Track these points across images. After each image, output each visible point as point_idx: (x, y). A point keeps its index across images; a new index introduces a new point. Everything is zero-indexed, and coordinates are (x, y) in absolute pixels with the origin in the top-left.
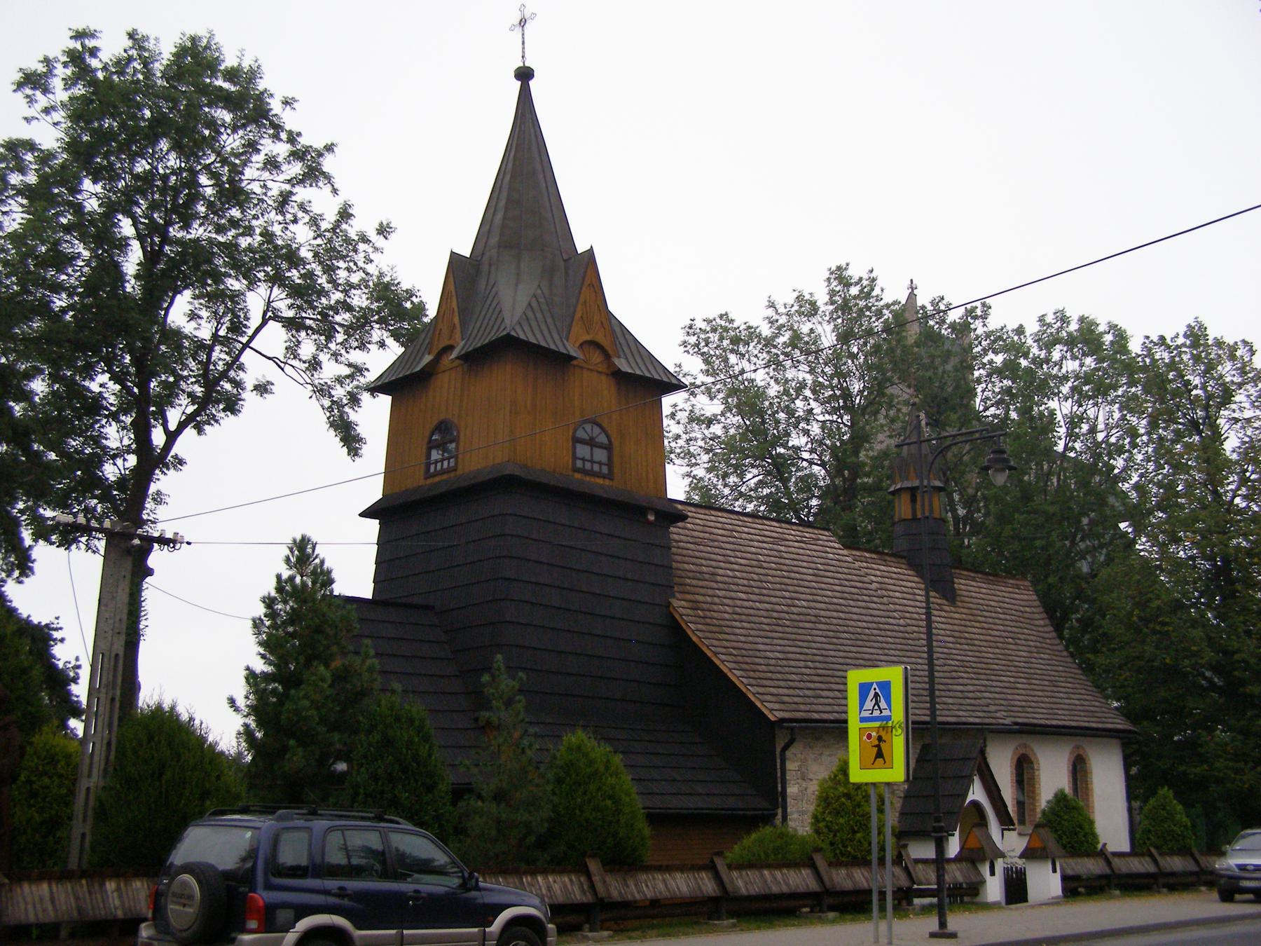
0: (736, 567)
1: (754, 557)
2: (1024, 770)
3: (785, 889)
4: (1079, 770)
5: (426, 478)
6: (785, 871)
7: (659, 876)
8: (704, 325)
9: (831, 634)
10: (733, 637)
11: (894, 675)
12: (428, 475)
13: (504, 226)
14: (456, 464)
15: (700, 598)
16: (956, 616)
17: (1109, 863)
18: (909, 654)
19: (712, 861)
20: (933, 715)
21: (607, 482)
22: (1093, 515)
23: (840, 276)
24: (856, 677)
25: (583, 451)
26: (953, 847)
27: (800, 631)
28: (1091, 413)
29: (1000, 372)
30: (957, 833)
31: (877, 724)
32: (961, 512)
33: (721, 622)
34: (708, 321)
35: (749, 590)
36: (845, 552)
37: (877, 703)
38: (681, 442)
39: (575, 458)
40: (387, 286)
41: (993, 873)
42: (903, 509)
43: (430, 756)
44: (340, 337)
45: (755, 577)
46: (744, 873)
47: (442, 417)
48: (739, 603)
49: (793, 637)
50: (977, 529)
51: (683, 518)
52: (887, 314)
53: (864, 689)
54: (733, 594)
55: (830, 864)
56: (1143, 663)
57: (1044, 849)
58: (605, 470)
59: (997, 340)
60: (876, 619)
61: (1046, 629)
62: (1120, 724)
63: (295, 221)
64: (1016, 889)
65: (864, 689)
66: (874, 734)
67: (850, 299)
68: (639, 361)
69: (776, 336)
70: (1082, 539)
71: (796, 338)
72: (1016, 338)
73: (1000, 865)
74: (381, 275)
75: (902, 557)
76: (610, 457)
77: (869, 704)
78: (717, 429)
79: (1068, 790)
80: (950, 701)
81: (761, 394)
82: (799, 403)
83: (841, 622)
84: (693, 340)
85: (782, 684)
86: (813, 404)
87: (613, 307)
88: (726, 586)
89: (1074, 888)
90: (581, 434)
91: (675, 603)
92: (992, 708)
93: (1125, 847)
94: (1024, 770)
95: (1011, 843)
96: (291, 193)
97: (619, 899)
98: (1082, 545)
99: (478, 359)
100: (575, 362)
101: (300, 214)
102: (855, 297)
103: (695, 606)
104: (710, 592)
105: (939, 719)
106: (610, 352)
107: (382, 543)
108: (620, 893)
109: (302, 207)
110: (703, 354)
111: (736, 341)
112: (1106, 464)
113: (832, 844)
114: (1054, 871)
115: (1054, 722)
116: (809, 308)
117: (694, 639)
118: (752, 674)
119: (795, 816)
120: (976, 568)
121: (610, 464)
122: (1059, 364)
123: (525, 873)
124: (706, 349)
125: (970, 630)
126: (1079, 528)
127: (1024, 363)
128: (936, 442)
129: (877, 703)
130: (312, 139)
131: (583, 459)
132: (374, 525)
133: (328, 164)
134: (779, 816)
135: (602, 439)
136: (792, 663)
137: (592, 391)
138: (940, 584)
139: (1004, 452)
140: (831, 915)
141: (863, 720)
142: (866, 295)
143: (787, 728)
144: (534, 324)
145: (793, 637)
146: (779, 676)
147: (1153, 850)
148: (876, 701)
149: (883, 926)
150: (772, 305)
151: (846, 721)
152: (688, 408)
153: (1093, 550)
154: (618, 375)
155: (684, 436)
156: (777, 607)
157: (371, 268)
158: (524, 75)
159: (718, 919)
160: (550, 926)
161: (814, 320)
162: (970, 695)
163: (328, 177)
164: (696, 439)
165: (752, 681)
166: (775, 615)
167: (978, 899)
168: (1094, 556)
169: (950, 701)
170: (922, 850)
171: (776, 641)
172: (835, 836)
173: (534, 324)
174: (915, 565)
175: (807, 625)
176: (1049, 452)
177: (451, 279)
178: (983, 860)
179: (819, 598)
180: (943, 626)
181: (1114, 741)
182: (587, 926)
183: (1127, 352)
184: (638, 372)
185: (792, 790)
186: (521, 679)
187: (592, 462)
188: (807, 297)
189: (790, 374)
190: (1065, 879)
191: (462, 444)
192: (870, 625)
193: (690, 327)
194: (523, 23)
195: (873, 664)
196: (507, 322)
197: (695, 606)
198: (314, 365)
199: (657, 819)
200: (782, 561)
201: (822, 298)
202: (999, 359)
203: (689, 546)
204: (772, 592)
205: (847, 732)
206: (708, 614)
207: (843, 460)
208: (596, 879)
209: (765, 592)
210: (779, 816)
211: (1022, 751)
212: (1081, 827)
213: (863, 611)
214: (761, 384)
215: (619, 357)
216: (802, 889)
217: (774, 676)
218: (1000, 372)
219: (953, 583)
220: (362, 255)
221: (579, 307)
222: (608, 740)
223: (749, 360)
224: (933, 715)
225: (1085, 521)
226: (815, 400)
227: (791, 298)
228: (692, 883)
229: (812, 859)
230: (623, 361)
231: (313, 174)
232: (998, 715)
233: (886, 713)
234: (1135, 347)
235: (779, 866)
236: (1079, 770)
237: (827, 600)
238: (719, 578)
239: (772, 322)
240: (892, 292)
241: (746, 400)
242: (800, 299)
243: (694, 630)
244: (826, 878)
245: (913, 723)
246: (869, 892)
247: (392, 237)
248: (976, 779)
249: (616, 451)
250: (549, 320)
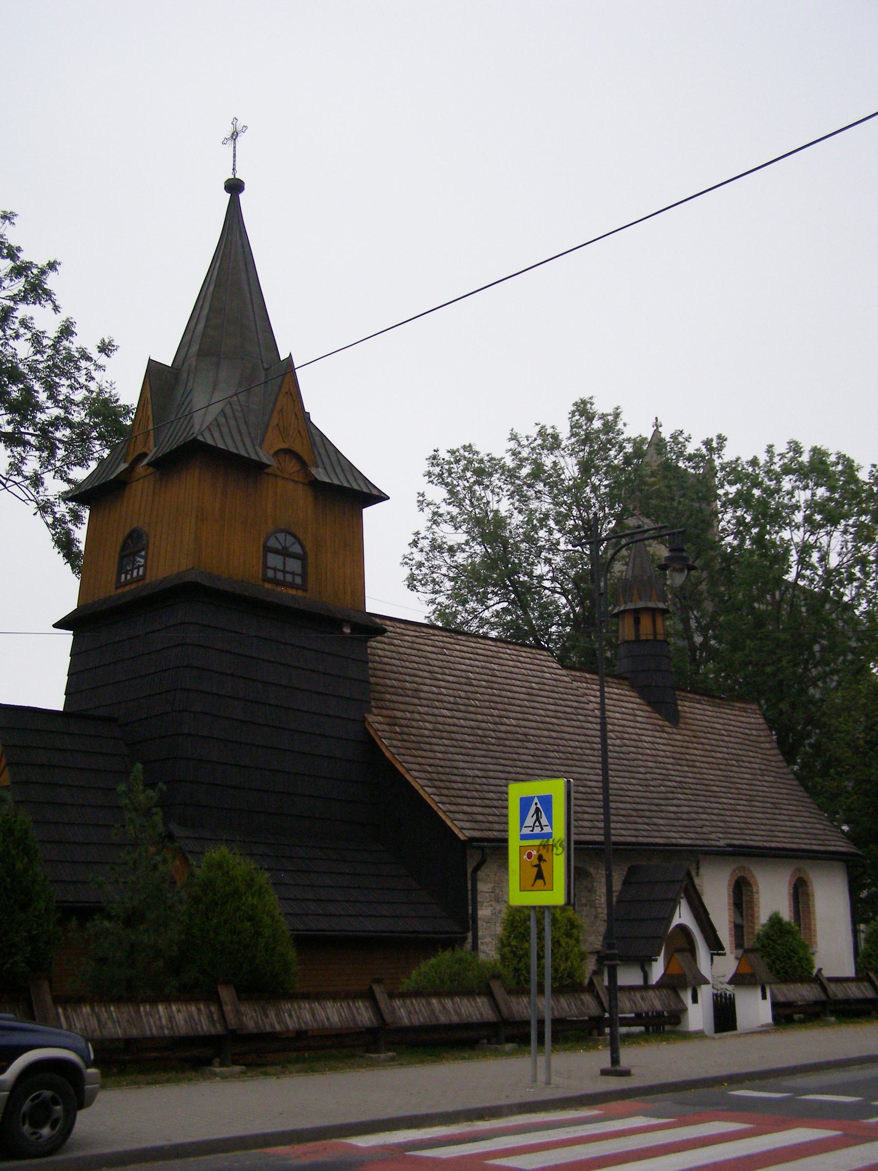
0: (442, 684)
1: (463, 674)
2: (742, 895)
3: (455, 1019)
4: (800, 894)
5: (117, 588)
6: (457, 999)
7: (305, 1005)
8: (447, 456)
9: (539, 753)
10: (430, 754)
11: (555, 789)
12: (119, 585)
13: (204, 334)
14: (145, 572)
15: (399, 714)
16: (678, 737)
17: (824, 989)
18: (622, 774)
19: (371, 989)
20: (607, 834)
21: (300, 593)
22: (825, 642)
23: (583, 409)
24: (516, 791)
25: (274, 560)
26: (657, 970)
27: (505, 749)
28: (824, 540)
29: (734, 503)
30: (661, 959)
31: (537, 842)
32: (698, 639)
33: (420, 739)
34: (453, 452)
35: (455, 707)
36: (564, 672)
37: (538, 819)
38: (424, 570)
39: (266, 567)
40: (106, 402)
41: (695, 1000)
42: (627, 631)
43: (26, 870)
44: (61, 453)
45: (462, 694)
46: (408, 1002)
47: (135, 525)
48: (441, 719)
49: (498, 754)
50: (713, 654)
51: (382, 631)
52: (629, 448)
53: (525, 803)
54: (436, 711)
55: (510, 992)
56: (868, 787)
57: (753, 975)
58: (298, 580)
59: (734, 473)
60: (589, 739)
61: (773, 752)
62: (843, 846)
63: (17, 336)
64: (725, 1016)
65: (525, 803)
66: (534, 853)
67: (594, 432)
68: (338, 470)
69: (520, 467)
70: (815, 667)
71: (538, 472)
72: (750, 469)
73: (705, 993)
74: (101, 391)
75: (626, 679)
76: (304, 567)
77: (530, 820)
78: (460, 558)
79: (786, 915)
80: (661, 822)
81: (500, 522)
82: (542, 533)
83: (551, 741)
84: (437, 470)
85: (478, 802)
86: (557, 535)
87: (316, 420)
88: (429, 703)
89: (785, 1015)
90: (273, 543)
91: (371, 718)
92: (705, 830)
93: (848, 970)
94: (742, 895)
95: (716, 969)
96: (13, 310)
97: (255, 1031)
98: (814, 672)
99: (170, 464)
100: (268, 470)
101: (22, 331)
102: (598, 431)
103: (393, 722)
104: (411, 708)
105: (613, 839)
106: (306, 458)
107: (75, 654)
108: (257, 1023)
109: (24, 323)
110: (447, 484)
111: (480, 473)
112: (837, 592)
113: (516, 970)
114: (764, 997)
115: (773, 845)
116: (551, 442)
117: (387, 754)
118: (445, 792)
119: (488, 940)
120: (707, 693)
121: (304, 575)
122: (791, 493)
123: (144, 1001)
124: (449, 480)
125: (691, 751)
126: (812, 655)
127: (756, 492)
128: (660, 564)
129: (538, 819)
130: (34, 254)
131: (275, 569)
132: (67, 638)
133: (51, 282)
134: (470, 940)
135: (297, 549)
136: (492, 781)
137: (286, 500)
138: (663, 706)
139: (683, 550)
140: (509, 1046)
141: (523, 837)
142: (609, 427)
143: (478, 848)
144: (225, 430)
145: (498, 754)
146: (475, 794)
147: (872, 975)
148: (536, 817)
149: (541, 1060)
150: (514, 437)
151: (506, 841)
152: (430, 536)
153: (823, 677)
154: (315, 485)
155: (427, 564)
156: (484, 725)
157: (93, 386)
158: (234, 187)
159: (377, 1051)
160: (92, 1070)
161: (556, 452)
162: (684, 816)
163: (48, 294)
164: (439, 567)
165: (444, 799)
166: (480, 732)
167: (680, 1028)
168: (825, 683)
169: (661, 822)
170: (628, 977)
171: (477, 759)
172: (519, 962)
173: (225, 430)
174: (634, 687)
175: (514, 743)
176: (779, 581)
177: (148, 388)
178: (684, 987)
179: (531, 717)
180: (663, 747)
181: (836, 863)
182: (218, 1060)
183: (856, 481)
184: (336, 482)
185: (484, 912)
186: (160, 789)
187: (284, 571)
188: (550, 431)
189: (534, 504)
190: (775, 1005)
191: (150, 551)
192: (583, 745)
193: (434, 458)
194: (234, 136)
195: (528, 777)
196: (196, 428)
197: (393, 722)
198: (36, 481)
199: (306, 942)
200: (494, 679)
201: (564, 432)
202: (732, 490)
203: (394, 661)
204: (479, 710)
205: (507, 848)
206: (405, 729)
207: (587, 586)
208: (228, 1008)
209: (471, 709)
210: (470, 940)
211: (740, 874)
212: (795, 952)
213: (577, 731)
214: (504, 514)
215: (317, 467)
216: (475, 1018)
217: (469, 794)
218: (734, 503)
219: (677, 705)
220: (84, 372)
221: (275, 414)
222: (251, 855)
223: (492, 491)
224: (607, 834)
225: (817, 648)
226: (560, 531)
227: (534, 432)
228: (345, 1013)
229: (488, 986)
230: (321, 470)
231: (37, 291)
232: (713, 836)
233: (547, 830)
234: (863, 476)
235: (450, 994)
236: (800, 894)
237: (538, 719)
238: (422, 695)
239: (515, 454)
240: (635, 427)
241: (489, 529)
242: (542, 433)
243: (388, 745)
244: (503, 1007)
245: (576, 842)
246: (528, 1023)
247: (115, 355)
248: (684, 902)
249: (311, 559)
250: (243, 428)
